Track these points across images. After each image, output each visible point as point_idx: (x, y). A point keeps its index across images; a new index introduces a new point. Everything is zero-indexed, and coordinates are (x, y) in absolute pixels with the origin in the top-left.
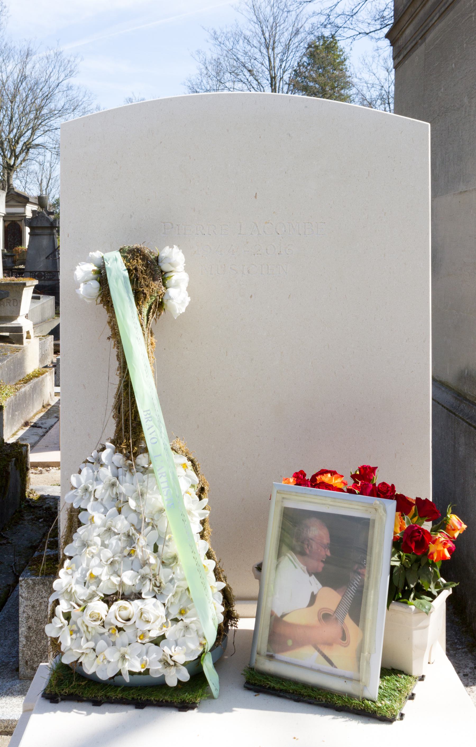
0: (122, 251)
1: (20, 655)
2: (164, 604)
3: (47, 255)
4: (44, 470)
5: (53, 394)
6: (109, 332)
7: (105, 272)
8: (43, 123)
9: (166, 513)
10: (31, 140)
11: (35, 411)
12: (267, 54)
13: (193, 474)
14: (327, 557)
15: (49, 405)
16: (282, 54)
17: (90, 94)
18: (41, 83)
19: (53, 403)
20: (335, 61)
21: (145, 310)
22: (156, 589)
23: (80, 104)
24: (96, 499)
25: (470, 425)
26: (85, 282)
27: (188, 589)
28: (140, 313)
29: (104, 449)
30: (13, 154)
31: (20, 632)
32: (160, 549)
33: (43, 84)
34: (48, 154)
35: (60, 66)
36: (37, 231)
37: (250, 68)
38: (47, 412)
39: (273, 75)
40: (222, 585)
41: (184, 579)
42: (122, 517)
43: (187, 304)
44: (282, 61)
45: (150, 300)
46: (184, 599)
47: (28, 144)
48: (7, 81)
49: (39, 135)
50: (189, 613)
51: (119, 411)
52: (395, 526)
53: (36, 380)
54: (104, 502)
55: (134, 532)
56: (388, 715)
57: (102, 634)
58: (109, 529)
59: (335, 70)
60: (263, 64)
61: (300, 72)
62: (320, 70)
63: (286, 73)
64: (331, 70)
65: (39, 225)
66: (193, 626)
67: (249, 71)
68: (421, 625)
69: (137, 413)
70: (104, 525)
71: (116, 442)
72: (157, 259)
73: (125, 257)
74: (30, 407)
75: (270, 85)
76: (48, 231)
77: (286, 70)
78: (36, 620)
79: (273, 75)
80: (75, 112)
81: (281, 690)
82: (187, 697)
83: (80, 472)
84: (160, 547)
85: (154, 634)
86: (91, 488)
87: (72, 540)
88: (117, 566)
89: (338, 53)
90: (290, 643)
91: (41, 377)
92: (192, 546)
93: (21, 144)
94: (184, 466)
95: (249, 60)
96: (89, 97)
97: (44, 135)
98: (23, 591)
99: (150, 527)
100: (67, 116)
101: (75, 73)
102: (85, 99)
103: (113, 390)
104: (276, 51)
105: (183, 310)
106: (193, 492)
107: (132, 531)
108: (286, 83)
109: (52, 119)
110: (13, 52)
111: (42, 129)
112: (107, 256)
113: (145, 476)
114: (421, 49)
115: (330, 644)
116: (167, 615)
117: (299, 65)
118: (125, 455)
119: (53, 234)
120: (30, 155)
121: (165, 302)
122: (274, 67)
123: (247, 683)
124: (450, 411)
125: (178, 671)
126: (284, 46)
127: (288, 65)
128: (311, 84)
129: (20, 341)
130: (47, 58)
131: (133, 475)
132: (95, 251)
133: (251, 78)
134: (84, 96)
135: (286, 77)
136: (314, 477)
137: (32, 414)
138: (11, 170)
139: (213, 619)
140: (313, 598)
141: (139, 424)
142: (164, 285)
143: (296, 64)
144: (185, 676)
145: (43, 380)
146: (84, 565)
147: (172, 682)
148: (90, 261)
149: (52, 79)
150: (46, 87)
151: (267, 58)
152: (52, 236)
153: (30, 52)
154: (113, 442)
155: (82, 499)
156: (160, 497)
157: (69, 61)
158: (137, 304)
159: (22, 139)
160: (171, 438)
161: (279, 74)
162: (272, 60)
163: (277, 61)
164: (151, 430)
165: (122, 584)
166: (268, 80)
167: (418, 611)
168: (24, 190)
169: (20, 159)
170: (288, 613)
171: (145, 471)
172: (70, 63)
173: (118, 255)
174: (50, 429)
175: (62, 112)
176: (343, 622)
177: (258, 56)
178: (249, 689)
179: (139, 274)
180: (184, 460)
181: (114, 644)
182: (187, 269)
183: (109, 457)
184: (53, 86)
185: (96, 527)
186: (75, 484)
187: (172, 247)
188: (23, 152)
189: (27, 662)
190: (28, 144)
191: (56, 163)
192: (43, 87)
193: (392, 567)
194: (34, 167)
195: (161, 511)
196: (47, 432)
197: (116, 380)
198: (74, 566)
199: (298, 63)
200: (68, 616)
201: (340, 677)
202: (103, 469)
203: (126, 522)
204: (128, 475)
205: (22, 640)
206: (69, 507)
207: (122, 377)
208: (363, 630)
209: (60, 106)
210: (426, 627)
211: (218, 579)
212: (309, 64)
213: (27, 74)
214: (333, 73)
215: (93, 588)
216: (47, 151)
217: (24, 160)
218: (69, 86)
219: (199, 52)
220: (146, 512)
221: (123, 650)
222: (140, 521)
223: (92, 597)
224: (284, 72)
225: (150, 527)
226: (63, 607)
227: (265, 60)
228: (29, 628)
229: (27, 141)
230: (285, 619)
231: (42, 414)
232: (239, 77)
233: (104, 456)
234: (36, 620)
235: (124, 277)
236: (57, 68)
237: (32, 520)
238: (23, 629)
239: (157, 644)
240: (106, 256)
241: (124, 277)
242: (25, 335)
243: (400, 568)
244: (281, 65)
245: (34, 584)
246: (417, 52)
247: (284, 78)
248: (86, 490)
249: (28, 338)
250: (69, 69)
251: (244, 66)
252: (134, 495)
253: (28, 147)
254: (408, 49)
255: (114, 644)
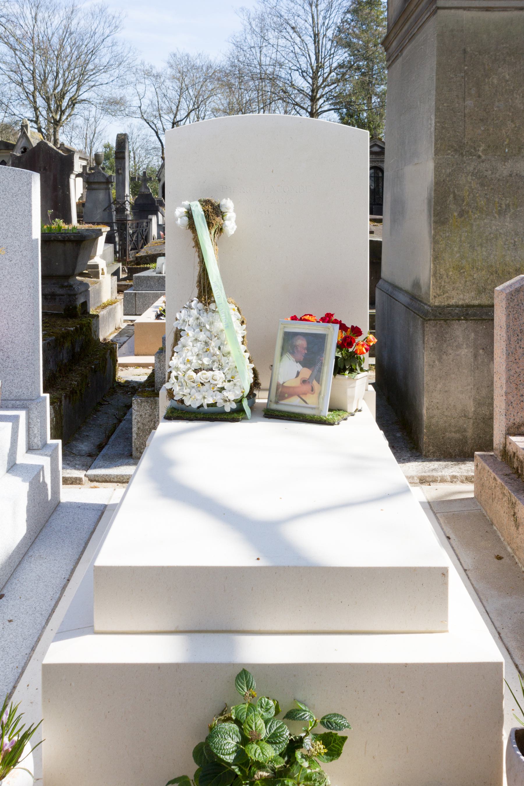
0: (200, 201)
1: (133, 444)
2: (224, 373)
3: (105, 207)
4: (124, 369)
5: (123, 321)
6: (193, 244)
7: (191, 212)
8: (89, 79)
9: (225, 332)
10: (76, 96)
11: (110, 331)
12: (310, 11)
13: (238, 313)
14: (306, 354)
15: (120, 328)
16: (325, 11)
17: (135, 50)
18: (86, 39)
19: (123, 327)
20: (378, 17)
21: (213, 232)
22: (220, 367)
23: (125, 59)
24: (189, 325)
25: (415, 313)
26: (181, 218)
27: (236, 367)
28: (211, 233)
29: (192, 301)
30: (59, 109)
31: (133, 431)
32: (221, 349)
33: (88, 40)
34: (93, 109)
35: (105, 22)
36: (94, 186)
37: (294, 25)
38: (119, 333)
39: (317, 32)
40: (253, 366)
41: (234, 362)
42: (203, 333)
43: (235, 229)
44: (325, 18)
45: (215, 227)
46: (234, 371)
47: (74, 100)
48: (52, 37)
49: (85, 90)
50: (236, 377)
51: (200, 283)
52: (338, 336)
53: (111, 307)
54: (193, 326)
55: (209, 340)
56: (332, 422)
57: (193, 387)
58: (196, 339)
59: (378, 26)
60: (306, 21)
61: (343, 29)
62: (364, 26)
63: (329, 30)
64: (375, 26)
65: (96, 181)
66: (238, 384)
67: (293, 28)
68: (351, 386)
69: (209, 284)
70: (194, 337)
71: (199, 297)
72: (219, 206)
73: (202, 204)
74: (107, 328)
75: (313, 42)
76: (103, 186)
77: (329, 28)
78: (143, 424)
79: (317, 32)
80: (120, 68)
81: (281, 416)
82: (235, 415)
83: (181, 312)
84: (222, 347)
85: (220, 386)
86: (187, 320)
87: (177, 344)
88: (200, 356)
89: (382, 10)
90: (286, 395)
91: (114, 305)
92: (239, 348)
93: (67, 98)
94: (234, 310)
95: (292, 17)
96: (134, 53)
97: (89, 91)
98: (135, 406)
99: (217, 338)
100: (113, 71)
101: (119, 29)
102: (130, 55)
103: (197, 273)
104: (319, 8)
105: (233, 233)
106: (239, 323)
107: (208, 340)
108: (330, 40)
109: (97, 74)
110: (58, 8)
111: (87, 84)
112: (192, 204)
113: (214, 314)
114: (400, 60)
115: (305, 394)
116: (226, 378)
117: (343, 22)
118: (203, 304)
119: (109, 189)
120: (76, 111)
121: (223, 228)
122: (318, 24)
123: (265, 414)
124: (407, 307)
125: (231, 404)
126: (327, 4)
127: (331, 22)
128: (355, 40)
129: (97, 275)
130: (92, 14)
131: (207, 313)
132: (185, 201)
133: (294, 35)
134: (129, 52)
135: (330, 34)
136: (301, 318)
137: (108, 334)
138: (57, 125)
139: (248, 381)
140: (298, 373)
141: (211, 289)
142: (223, 219)
143: (339, 20)
144: (234, 406)
145: (115, 308)
146: (184, 355)
147: (228, 409)
148: (183, 206)
149: (97, 35)
150: (91, 43)
151: (310, 15)
152: (107, 191)
153: (75, 8)
154: (197, 298)
155: (182, 325)
156: (221, 324)
157: (114, 17)
158: (209, 229)
159: (68, 94)
160: (227, 297)
161: (322, 32)
162: (315, 17)
163: (321, 18)
164: (217, 292)
165: (203, 364)
166: (311, 37)
167: (349, 378)
168: (69, 145)
169: (67, 114)
170: (281, 360)
171: (214, 311)
172: (115, 19)
173: (198, 203)
174: (124, 343)
175: (106, 68)
176: (312, 383)
177: (301, 12)
178: (266, 417)
179: (210, 214)
180: (234, 306)
181: (199, 391)
182: (235, 211)
183: (196, 305)
184: (98, 42)
185: (190, 337)
186: (178, 318)
187: (227, 199)
188: (69, 107)
189: (137, 449)
190: (74, 100)
191: (101, 117)
192: (88, 43)
193: (337, 358)
194: (79, 121)
195: (222, 331)
196: (122, 345)
197: (197, 269)
198: (179, 356)
199: (342, 20)
200: (177, 378)
201: (309, 408)
202: (192, 310)
203: (204, 336)
204: (205, 313)
205: (134, 435)
206: (175, 330)
207: (201, 266)
208: (321, 385)
209: (104, 61)
210: (354, 387)
211: (250, 362)
212: (352, 21)
213: (72, 30)
214: (376, 30)
215: (189, 365)
216: (93, 106)
217: (70, 115)
218: (114, 41)
219: (242, 9)
220: (214, 331)
221: (204, 393)
222: (211, 336)
223: (188, 369)
224: (327, 30)
225: (217, 338)
226: (174, 374)
227: (308, 17)
228: (139, 428)
229: (73, 96)
230: (285, 385)
231: (116, 334)
232: (283, 34)
233: (193, 304)
234: (143, 424)
235: (202, 215)
236: (102, 24)
237: (123, 393)
238: (135, 429)
239: (220, 392)
240: (192, 204)
241: (202, 215)
242: (101, 272)
243: (341, 359)
244: (324, 23)
245: (142, 402)
246: (398, 60)
247: (328, 34)
248: (184, 321)
249: (103, 274)
250: (114, 25)
251: (288, 23)
252: (209, 323)
253: (73, 102)
254: (394, 57)
255: (199, 391)
